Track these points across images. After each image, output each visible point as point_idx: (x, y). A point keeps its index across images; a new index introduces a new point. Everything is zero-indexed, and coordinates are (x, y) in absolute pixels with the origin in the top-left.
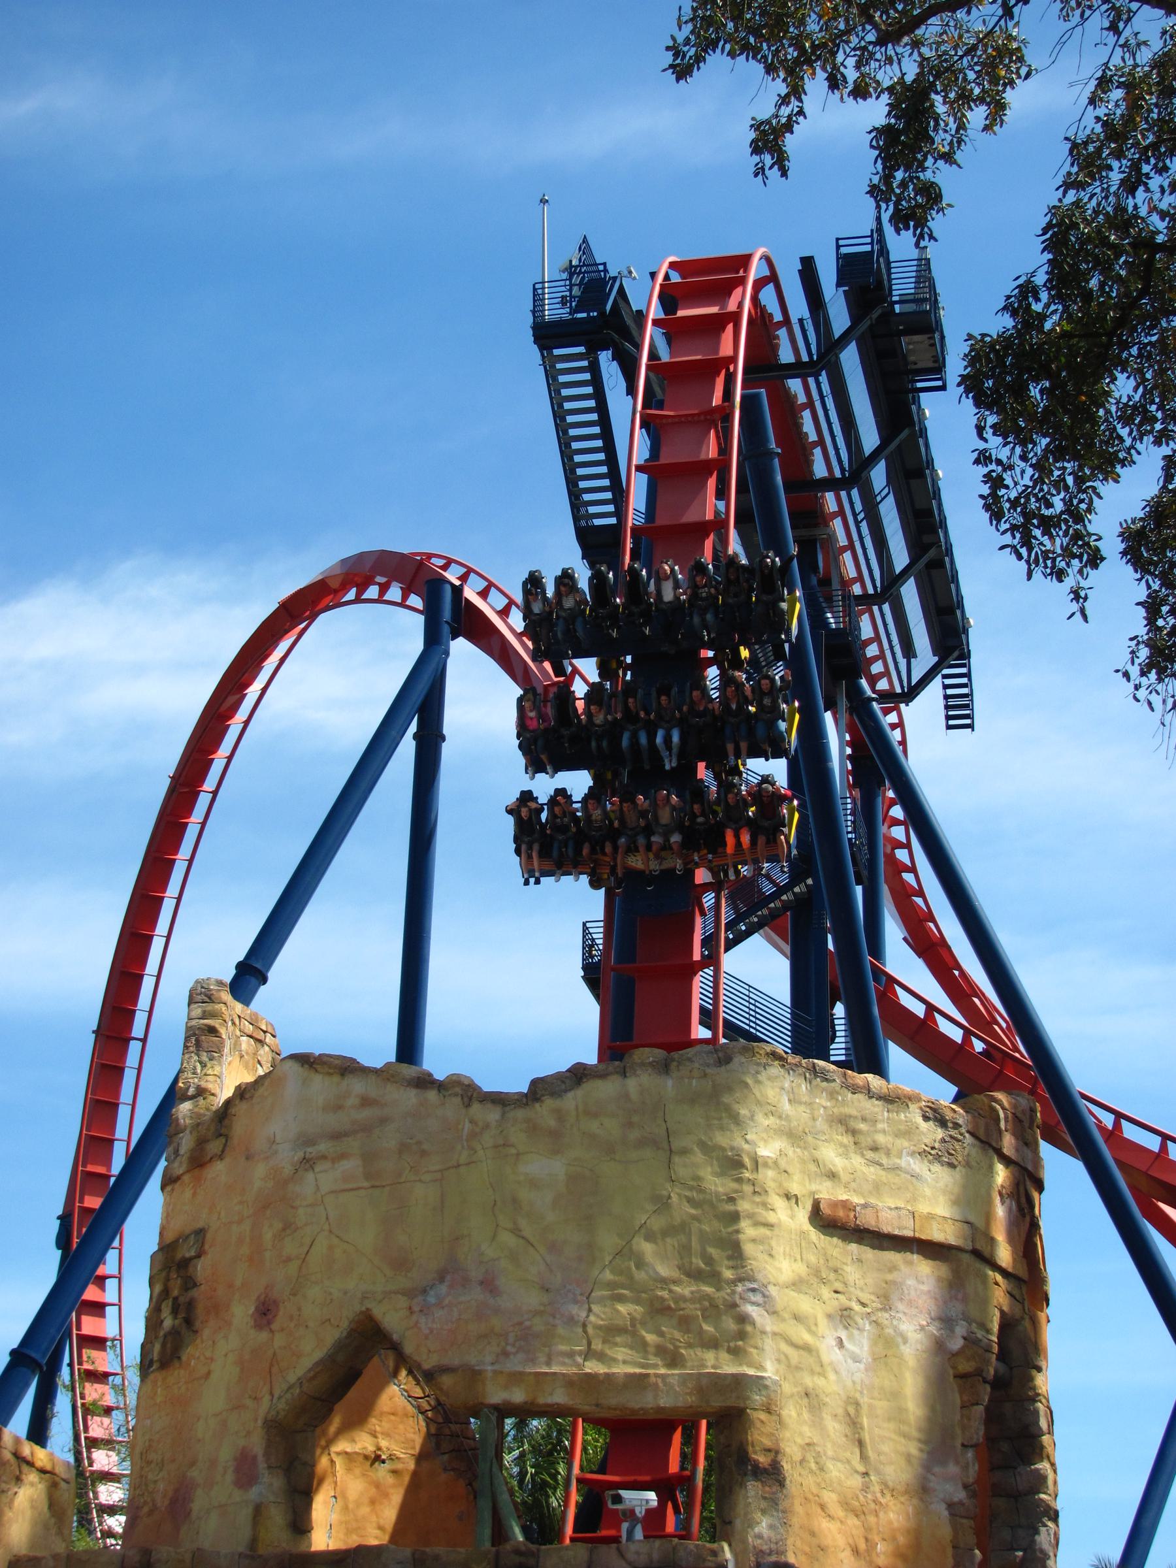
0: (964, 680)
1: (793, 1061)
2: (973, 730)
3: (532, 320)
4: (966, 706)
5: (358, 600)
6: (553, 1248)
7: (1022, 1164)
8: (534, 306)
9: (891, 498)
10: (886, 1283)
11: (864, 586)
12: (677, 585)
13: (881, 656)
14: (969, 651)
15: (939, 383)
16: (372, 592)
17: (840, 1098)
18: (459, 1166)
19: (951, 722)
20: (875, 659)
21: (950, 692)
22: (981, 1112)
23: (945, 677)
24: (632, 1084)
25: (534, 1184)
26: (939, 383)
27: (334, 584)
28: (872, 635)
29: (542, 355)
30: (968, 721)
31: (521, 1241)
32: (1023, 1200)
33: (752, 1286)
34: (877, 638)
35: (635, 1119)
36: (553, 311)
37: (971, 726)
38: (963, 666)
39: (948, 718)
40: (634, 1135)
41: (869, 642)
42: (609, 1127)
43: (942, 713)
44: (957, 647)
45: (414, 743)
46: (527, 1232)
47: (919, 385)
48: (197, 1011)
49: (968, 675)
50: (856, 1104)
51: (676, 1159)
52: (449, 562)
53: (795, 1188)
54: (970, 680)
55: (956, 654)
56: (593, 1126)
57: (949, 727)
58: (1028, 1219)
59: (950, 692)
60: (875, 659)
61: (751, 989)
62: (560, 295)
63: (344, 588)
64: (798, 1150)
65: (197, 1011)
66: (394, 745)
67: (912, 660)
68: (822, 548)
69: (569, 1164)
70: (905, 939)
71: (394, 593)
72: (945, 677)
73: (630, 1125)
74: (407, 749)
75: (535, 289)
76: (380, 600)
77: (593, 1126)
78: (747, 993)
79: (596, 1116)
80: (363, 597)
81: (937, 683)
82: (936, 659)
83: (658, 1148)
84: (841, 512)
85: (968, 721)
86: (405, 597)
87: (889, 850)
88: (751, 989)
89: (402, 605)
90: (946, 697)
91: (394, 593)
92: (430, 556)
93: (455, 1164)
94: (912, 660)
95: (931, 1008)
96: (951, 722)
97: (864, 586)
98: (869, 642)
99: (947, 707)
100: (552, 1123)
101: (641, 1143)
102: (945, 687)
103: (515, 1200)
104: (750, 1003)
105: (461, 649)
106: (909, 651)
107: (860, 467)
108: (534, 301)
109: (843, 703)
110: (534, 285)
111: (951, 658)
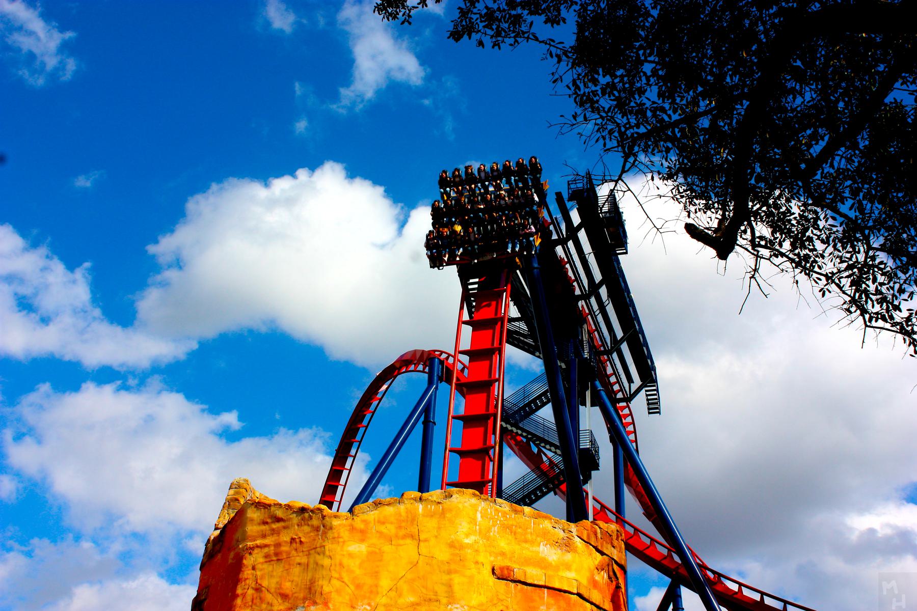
0: (655, 392)
1: (484, 498)
2: (660, 414)
6: (358, 587)
7: (610, 556)
9: (611, 304)
10: (530, 608)
11: (604, 348)
15: (625, 251)
17: (508, 516)
18: (316, 548)
21: (649, 397)
22: (585, 527)
23: (646, 391)
24: (402, 507)
25: (351, 555)
26: (625, 251)
27: (398, 365)
30: (658, 410)
31: (343, 584)
32: (611, 573)
33: (456, 606)
35: (403, 524)
37: (659, 413)
38: (654, 386)
39: (649, 409)
40: (402, 533)
42: (390, 529)
43: (646, 407)
45: (422, 426)
46: (346, 579)
47: (618, 252)
48: (232, 492)
49: (657, 390)
50: (517, 519)
51: (422, 544)
52: (442, 352)
53: (481, 559)
54: (658, 392)
56: (382, 528)
57: (649, 413)
58: (614, 583)
59: (649, 397)
63: (400, 368)
64: (485, 541)
65: (232, 492)
67: (632, 384)
69: (369, 547)
70: (643, 513)
71: (420, 367)
72: (646, 391)
73: (400, 527)
74: (420, 427)
77: (382, 528)
79: (383, 523)
81: (643, 392)
83: (413, 539)
85: (658, 410)
90: (648, 400)
91: (420, 367)
92: (435, 351)
93: (315, 547)
94: (632, 384)
95: (653, 540)
97: (604, 348)
99: (648, 404)
100: (362, 526)
101: (404, 537)
102: (647, 395)
103: (341, 564)
106: (630, 380)
107: (594, 288)
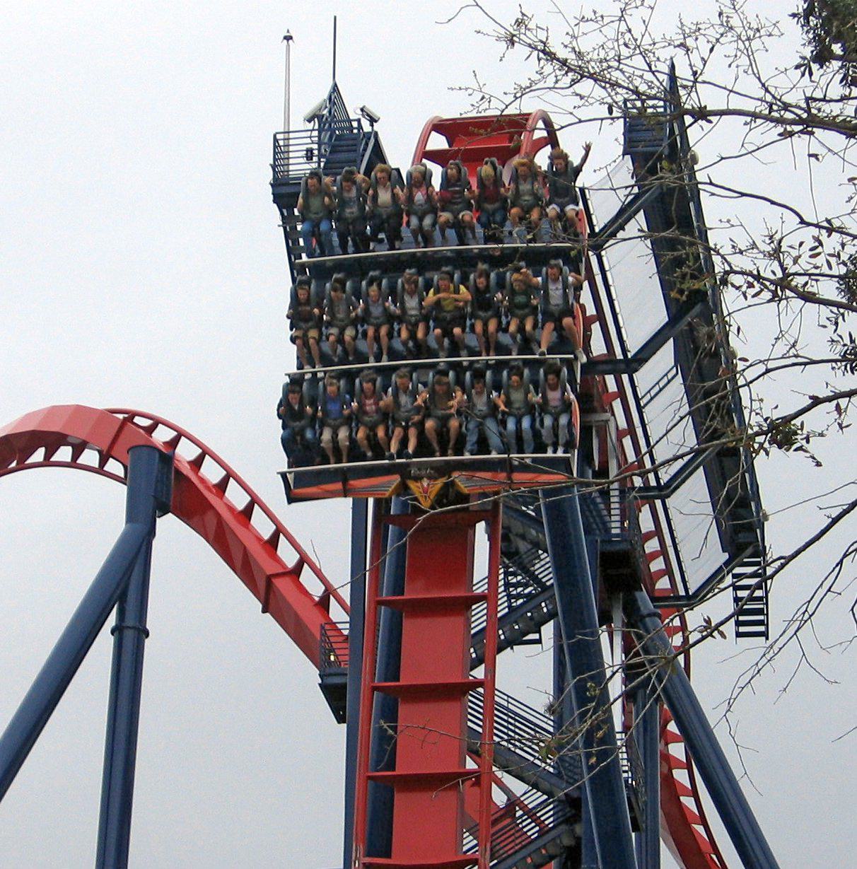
3: (272, 177)
4: (760, 612)
5: (47, 462)
8: (275, 159)
12: (408, 224)
13: (663, 552)
14: (765, 548)
16: (64, 453)
19: (742, 629)
20: (654, 556)
28: (653, 528)
29: (282, 214)
30: (762, 629)
34: (658, 532)
36: (299, 167)
37: (765, 635)
41: (648, 536)
44: (750, 543)
55: (750, 551)
57: (739, 635)
60: (654, 556)
61: (510, 700)
62: (304, 147)
66: (87, 645)
68: (598, 435)
71: (90, 457)
75: (276, 140)
76: (73, 464)
78: (505, 704)
80: (53, 459)
82: (726, 556)
84: (621, 394)
85: (762, 629)
86: (103, 461)
87: (666, 770)
88: (510, 700)
89: (100, 471)
91: (90, 457)
96: (742, 629)
98: (648, 536)
104: (514, 732)
105: (170, 528)
108: (275, 153)
109: (618, 617)
110: (275, 136)
111: (744, 555)
